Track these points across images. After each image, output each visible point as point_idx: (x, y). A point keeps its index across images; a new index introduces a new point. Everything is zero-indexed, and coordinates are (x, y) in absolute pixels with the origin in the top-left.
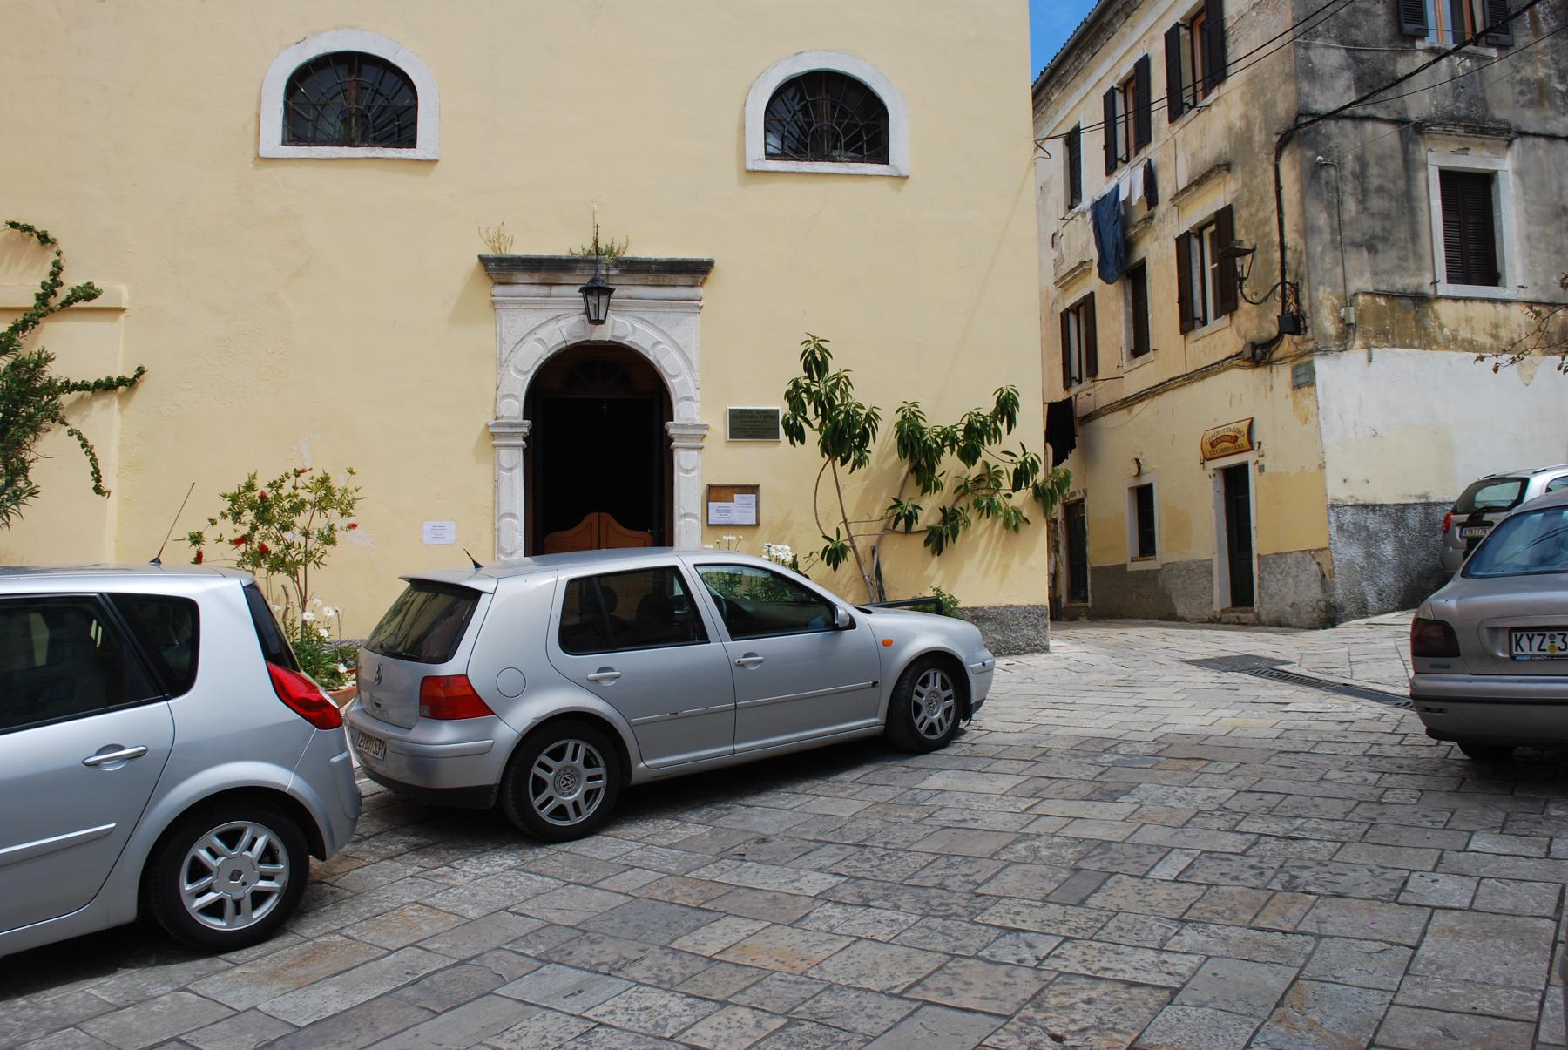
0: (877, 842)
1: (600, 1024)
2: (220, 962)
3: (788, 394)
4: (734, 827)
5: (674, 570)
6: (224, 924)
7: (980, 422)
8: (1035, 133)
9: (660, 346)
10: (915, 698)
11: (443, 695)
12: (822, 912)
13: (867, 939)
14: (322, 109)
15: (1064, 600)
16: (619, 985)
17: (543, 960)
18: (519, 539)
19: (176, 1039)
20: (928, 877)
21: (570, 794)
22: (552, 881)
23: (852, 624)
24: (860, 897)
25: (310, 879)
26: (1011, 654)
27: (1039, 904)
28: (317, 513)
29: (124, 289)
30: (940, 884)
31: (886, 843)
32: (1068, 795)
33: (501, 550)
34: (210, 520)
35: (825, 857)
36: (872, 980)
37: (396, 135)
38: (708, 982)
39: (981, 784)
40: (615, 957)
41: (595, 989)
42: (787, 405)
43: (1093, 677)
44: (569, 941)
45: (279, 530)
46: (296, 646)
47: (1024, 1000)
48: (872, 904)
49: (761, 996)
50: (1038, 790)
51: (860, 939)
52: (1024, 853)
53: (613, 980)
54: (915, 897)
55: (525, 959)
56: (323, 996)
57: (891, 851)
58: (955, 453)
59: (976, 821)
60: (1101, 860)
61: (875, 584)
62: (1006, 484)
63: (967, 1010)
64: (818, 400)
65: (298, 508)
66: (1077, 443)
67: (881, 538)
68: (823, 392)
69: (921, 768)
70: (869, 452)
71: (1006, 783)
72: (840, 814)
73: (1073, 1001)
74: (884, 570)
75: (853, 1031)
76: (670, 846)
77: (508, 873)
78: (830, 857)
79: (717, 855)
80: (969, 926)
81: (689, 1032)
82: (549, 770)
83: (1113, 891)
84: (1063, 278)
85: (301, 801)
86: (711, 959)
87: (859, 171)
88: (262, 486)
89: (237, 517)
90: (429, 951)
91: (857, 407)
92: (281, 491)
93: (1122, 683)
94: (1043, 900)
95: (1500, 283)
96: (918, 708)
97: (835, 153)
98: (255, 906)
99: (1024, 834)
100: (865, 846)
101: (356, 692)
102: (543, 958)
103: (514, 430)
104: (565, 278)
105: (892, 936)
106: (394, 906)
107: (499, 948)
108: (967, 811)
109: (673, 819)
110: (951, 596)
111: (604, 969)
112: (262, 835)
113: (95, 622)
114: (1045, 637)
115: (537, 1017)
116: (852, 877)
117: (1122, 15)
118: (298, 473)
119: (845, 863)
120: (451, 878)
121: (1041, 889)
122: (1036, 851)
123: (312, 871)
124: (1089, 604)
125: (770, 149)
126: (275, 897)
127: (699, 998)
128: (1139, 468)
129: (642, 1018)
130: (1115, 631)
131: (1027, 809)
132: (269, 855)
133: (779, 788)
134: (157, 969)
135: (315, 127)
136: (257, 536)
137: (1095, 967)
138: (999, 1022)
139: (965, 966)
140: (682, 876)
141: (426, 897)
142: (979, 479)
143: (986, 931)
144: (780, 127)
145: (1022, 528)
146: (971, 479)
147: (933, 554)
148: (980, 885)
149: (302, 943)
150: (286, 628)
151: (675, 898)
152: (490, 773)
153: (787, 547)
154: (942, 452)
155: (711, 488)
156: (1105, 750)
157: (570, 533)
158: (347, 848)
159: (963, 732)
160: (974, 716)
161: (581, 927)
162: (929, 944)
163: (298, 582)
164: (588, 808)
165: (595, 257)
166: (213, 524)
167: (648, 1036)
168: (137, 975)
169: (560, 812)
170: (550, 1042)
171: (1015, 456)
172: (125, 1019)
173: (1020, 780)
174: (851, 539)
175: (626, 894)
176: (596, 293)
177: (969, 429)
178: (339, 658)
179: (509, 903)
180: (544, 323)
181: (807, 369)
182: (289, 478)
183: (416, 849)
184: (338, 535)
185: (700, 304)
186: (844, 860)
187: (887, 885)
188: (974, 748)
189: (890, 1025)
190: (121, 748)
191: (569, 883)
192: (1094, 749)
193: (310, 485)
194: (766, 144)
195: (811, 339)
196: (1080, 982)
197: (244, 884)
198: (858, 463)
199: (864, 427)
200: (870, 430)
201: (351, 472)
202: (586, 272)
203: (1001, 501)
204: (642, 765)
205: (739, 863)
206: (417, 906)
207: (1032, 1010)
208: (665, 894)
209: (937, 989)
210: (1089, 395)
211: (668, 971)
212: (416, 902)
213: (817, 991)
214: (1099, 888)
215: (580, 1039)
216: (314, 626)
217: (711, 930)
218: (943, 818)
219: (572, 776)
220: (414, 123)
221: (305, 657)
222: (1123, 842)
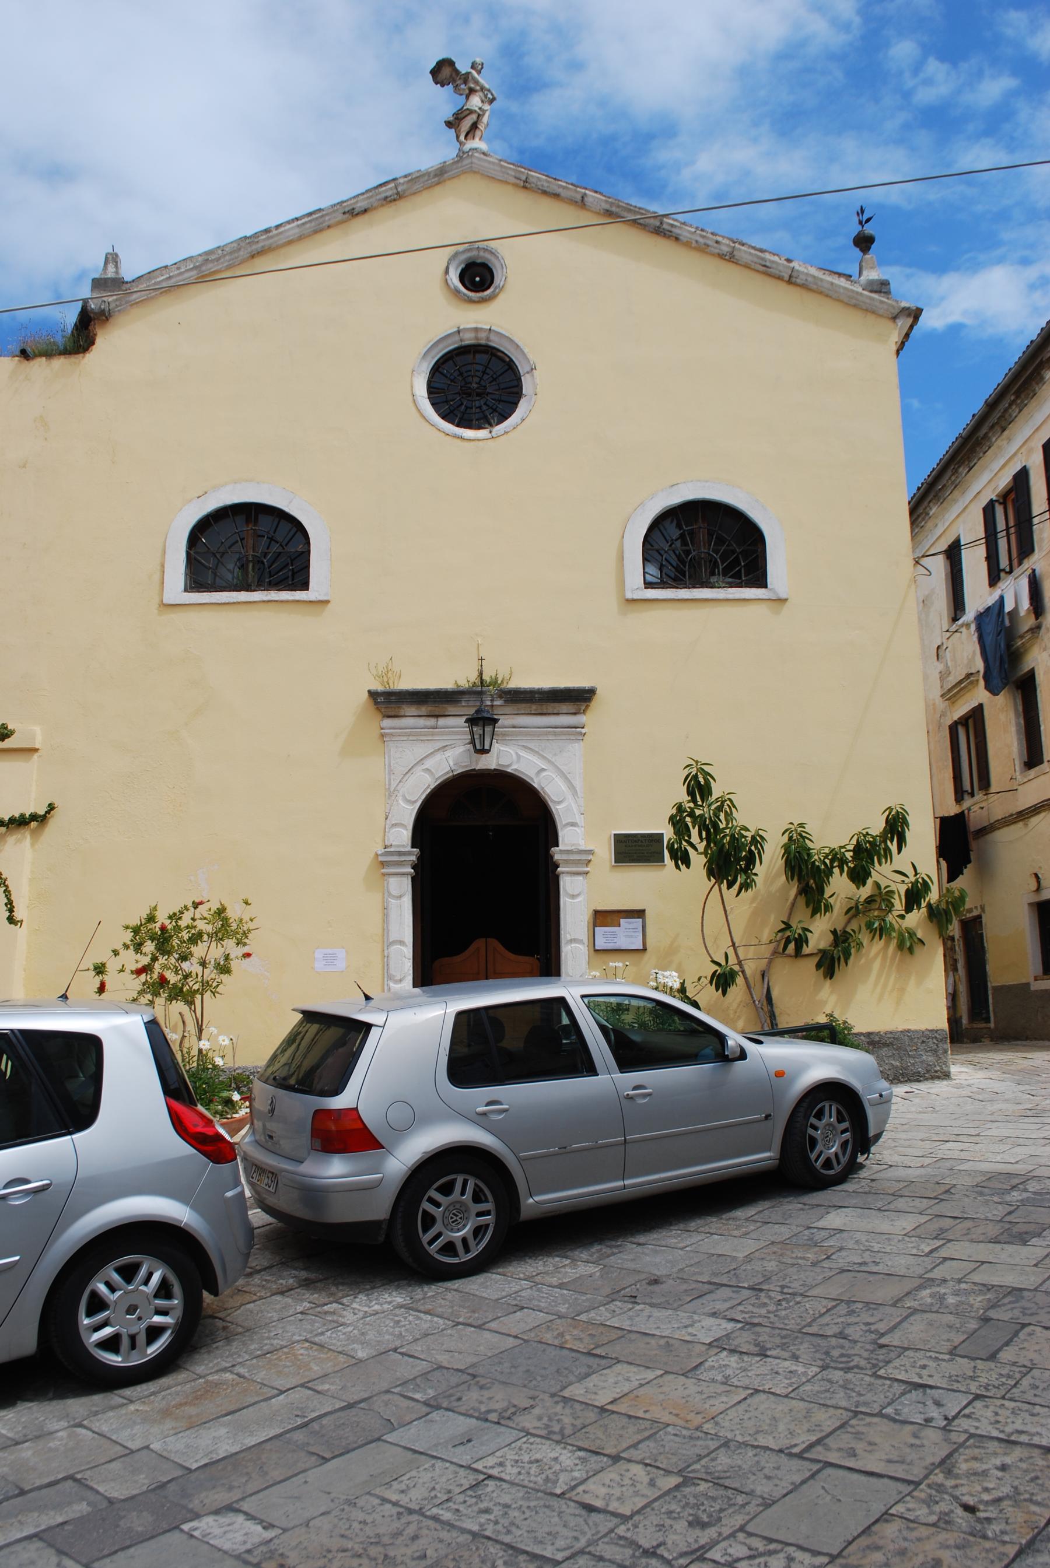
0: (773, 1286)
1: (490, 1477)
2: (115, 1398)
3: (672, 819)
4: (625, 1266)
5: (561, 1001)
6: (120, 1359)
7: (869, 842)
8: (914, 550)
9: (544, 774)
10: (810, 1131)
11: (333, 1128)
12: (717, 1361)
13: (764, 1392)
14: (221, 557)
15: (965, 1021)
16: (509, 1435)
17: (433, 1406)
18: (408, 965)
19: (71, 1477)
20: (828, 1325)
21: (459, 1230)
22: (441, 1321)
23: (743, 1055)
24: (756, 1345)
25: (203, 1313)
26: (909, 1081)
27: (947, 1357)
28: (214, 944)
29: (37, 729)
30: (841, 1333)
31: (783, 1287)
32: (974, 1236)
33: (390, 978)
34: (113, 951)
35: (719, 1301)
36: (770, 1438)
37: (290, 579)
38: (600, 1434)
39: (881, 1224)
40: (505, 1404)
41: (486, 1438)
42: (671, 829)
43: (997, 1106)
44: (458, 1385)
45: (177, 960)
46: (193, 1075)
47: (933, 1464)
48: (769, 1353)
49: (655, 1451)
50: (942, 1231)
51: (757, 1391)
52: (929, 1300)
53: (503, 1429)
54: (815, 1346)
55: (413, 1404)
56: (214, 1438)
57: (789, 1295)
58: (845, 874)
59: (877, 1264)
60: (1012, 1309)
61: (766, 1009)
62: (899, 905)
63: (872, 1474)
64: (702, 823)
65: (196, 938)
66: (972, 857)
67: (770, 962)
68: (707, 815)
69: (818, 1206)
70: (756, 874)
71: (907, 1223)
72: (734, 1254)
73: (985, 1467)
74: (775, 994)
75: (751, 1493)
76: (561, 1286)
77: (397, 1311)
78: (725, 1301)
79: (607, 1296)
80: (872, 1380)
81: (580, 1489)
82: (438, 1205)
83: (1026, 1345)
84: (950, 690)
85: (199, 1238)
86: (602, 1409)
87: (737, 596)
88: (162, 918)
89: (138, 947)
90: (319, 1392)
91: (742, 829)
92: (180, 923)
93: (1029, 1113)
94: (951, 1353)
96: (813, 1142)
97: (713, 579)
98: (150, 1341)
99: (929, 1279)
100: (761, 1290)
101: (249, 1119)
102: (432, 1403)
103: (403, 858)
104: (451, 709)
105: (791, 1389)
106: (284, 1343)
107: (388, 1392)
108: (868, 1252)
109: (563, 1257)
110: (845, 1022)
111: (493, 1417)
112: (157, 1270)
113: (5, 1057)
114: (945, 1063)
115: (426, 1466)
116: (747, 1323)
117: (997, 428)
118: (196, 905)
119: (740, 1308)
120: (340, 1316)
121: (948, 1340)
122: (942, 1298)
123: (205, 1305)
124: (992, 1025)
125: (649, 578)
126: (169, 1332)
127: (590, 1451)
128: (1039, 882)
129: (532, 1472)
130: (1020, 1054)
131: (931, 1252)
132: (164, 1290)
133: (671, 1225)
134: (54, 1403)
135: (215, 574)
136: (157, 966)
137: (1009, 1429)
138: (906, 1489)
139: (869, 1424)
140: (573, 1318)
141: (316, 1335)
142: (870, 900)
143: (890, 1387)
144: (659, 558)
145: (917, 949)
146: (862, 900)
147: (825, 977)
148: (883, 1335)
149: (195, 1380)
150: (183, 1056)
151: (566, 1342)
152: (379, 1209)
153: (674, 974)
154: (831, 873)
155: (597, 913)
156: (1013, 1188)
157: (457, 959)
158: (241, 1282)
159: (861, 1166)
160: (873, 1149)
161: (470, 1371)
162: (830, 1398)
163: (195, 1011)
164: (477, 1244)
165: (479, 689)
166: (115, 955)
167: (538, 1491)
168: (35, 1408)
169: (449, 1248)
170: (439, 1495)
171: (906, 876)
172: (23, 1455)
173: (923, 1219)
174: (740, 963)
175: (516, 1337)
176: (481, 723)
177: (858, 850)
178: (233, 1085)
179: (398, 1343)
180: (432, 753)
181: (691, 793)
182: (187, 910)
183: (307, 1284)
184: (234, 965)
185: (584, 731)
186: (740, 1304)
187: (784, 1332)
188: (874, 1184)
189: (791, 1487)
190: (27, 1181)
191: (459, 1323)
192: (1000, 1186)
193: (208, 916)
194: (644, 573)
195: (693, 763)
196: (993, 1446)
197: (140, 1319)
198: (746, 886)
199: (750, 849)
200: (756, 852)
201: (247, 903)
202: (471, 703)
203: (894, 922)
204: (531, 1200)
205: (630, 1306)
206: (307, 1344)
207: (941, 1476)
208: (556, 1338)
209: (840, 1450)
210: (982, 808)
211: (558, 1421)
212: (306, 1340)
213: (712, 1448)
214: (1011, 1340)
215: (470, 1493)
216: (210, 1054)
217: (603, 1378)
218: (842, 1260)
219: (459, 1213)
220: (307, 567)
221: (201, 1086)
222: (1035, 1290)
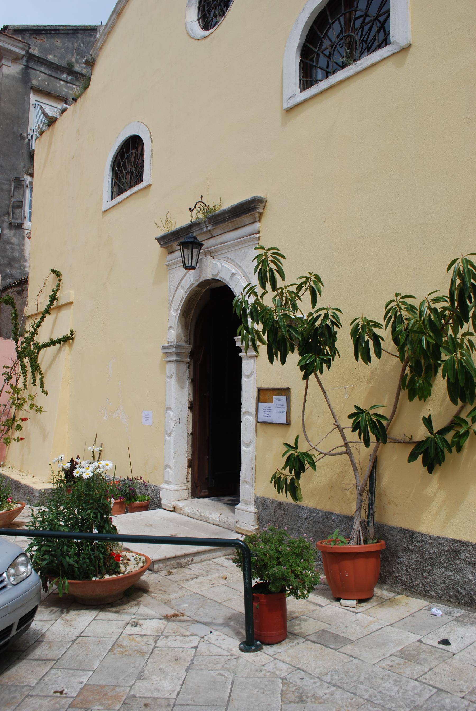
95: (388, 43)
155: (259, 390)
176: (190, 246)
